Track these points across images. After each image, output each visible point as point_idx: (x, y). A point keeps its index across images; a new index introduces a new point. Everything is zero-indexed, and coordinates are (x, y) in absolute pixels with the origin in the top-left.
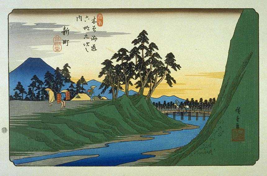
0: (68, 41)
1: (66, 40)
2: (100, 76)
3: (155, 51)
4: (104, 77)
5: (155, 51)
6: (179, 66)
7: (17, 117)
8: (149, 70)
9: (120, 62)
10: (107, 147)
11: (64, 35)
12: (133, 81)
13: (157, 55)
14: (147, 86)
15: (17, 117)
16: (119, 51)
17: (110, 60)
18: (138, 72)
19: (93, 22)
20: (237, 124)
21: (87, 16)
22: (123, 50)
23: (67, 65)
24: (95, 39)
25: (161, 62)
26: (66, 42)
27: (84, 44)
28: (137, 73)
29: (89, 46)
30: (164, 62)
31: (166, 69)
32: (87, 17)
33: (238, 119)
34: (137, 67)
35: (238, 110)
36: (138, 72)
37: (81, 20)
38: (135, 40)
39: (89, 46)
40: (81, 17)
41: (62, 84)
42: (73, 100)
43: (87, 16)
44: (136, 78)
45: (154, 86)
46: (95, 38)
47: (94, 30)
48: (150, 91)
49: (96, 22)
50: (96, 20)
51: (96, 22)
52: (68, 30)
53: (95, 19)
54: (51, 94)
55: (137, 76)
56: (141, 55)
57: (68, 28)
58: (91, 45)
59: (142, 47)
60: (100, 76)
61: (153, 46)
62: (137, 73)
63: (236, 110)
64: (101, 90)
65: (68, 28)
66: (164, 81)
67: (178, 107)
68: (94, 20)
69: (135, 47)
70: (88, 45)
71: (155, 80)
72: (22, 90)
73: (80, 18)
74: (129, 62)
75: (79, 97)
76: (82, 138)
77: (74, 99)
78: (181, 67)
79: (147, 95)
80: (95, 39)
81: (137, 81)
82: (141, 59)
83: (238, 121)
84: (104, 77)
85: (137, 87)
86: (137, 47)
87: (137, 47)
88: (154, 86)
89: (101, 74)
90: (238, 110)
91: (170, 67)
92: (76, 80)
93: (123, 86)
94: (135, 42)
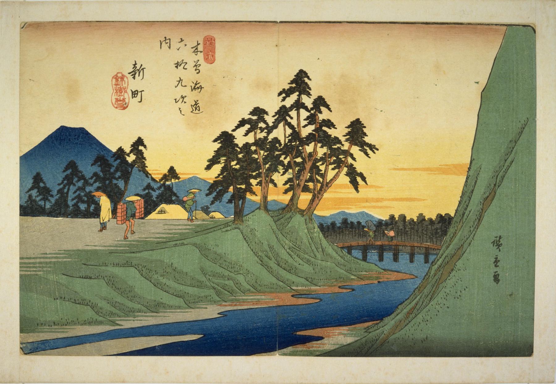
0: (141, 92)
1: (137, 91)
2: (208, 168)
3: (324, 115)
4: (217, 169)
5: (324, 115)
6: (372, 147)
7: (184, 312)
8: (310, 155)
9: (250, 139)
10: (224, 316)
11: (134, 78)
12: (280, 178)
13: (329, 124)
14: (306, 189)
15: (187, 312)
16: (252, 113)
17: (230, 132)
18: (288, 159)
19: (194, 52)
20: (495, 272)
21: (181, 39)
22: (259, 112)
23: (140, 142)
24: (198, 88)
25: (337, 140)
26: (137, 94)
27: (176, 99)
28: (286, 162)
29: (185, 102)
30: (343, 139)
31: (347, 153)
32: (182, 40)
33: (496, 261)
34: (288, 150)
35: (497, 243)
36: (288, 159)
37: (170, 48)
38: (284, 91)
39: (185, 102)
40: (170, 39)
41: (351, 246)
42: (150, 217)
43: (181, 39)
44: (284, 173)
45: (321, 190)
46: (198, 86)
47: (196, 70)
48: (312, 200)
49: (201, 52)
50: (200, 48)
51: (201, 52)
52: (143, 69)
53: (199, 46)
54: (105, 203)
55: (286, 168)
56: (294, 122)
57: (142, 65)
58: (190, 100)
59: (299, 105)
60: (208, 168)
61: (320, 102)
62: (286, 162)
63: (493, 242)
64: (211, 197)
65: (142, 65)
66: (344, 179)
67: (371, 233)
68: (197, 49)
69: (284, 107)
70: (184, 100)
71: (323, 176)
72: (45, 192)
73: (167, 43)
74: (271, 137)
75: (162, 212)
76: (166, 298)
77: (153, 216)
78: (377, 150)
79: (305, 209)
80: (198, 88)
81: (287, 176)
82: (295, 135)
83: (496, 266)
84: (217, 169)
85: (286, 192)
86: (288, 106)
87: (288, 106)
88: (322, 190)
89: (213, 162)
90: (497, 243)
91: (355, 150)
92: (158, 174)
93: (257, 189)
94: (287, 93)
